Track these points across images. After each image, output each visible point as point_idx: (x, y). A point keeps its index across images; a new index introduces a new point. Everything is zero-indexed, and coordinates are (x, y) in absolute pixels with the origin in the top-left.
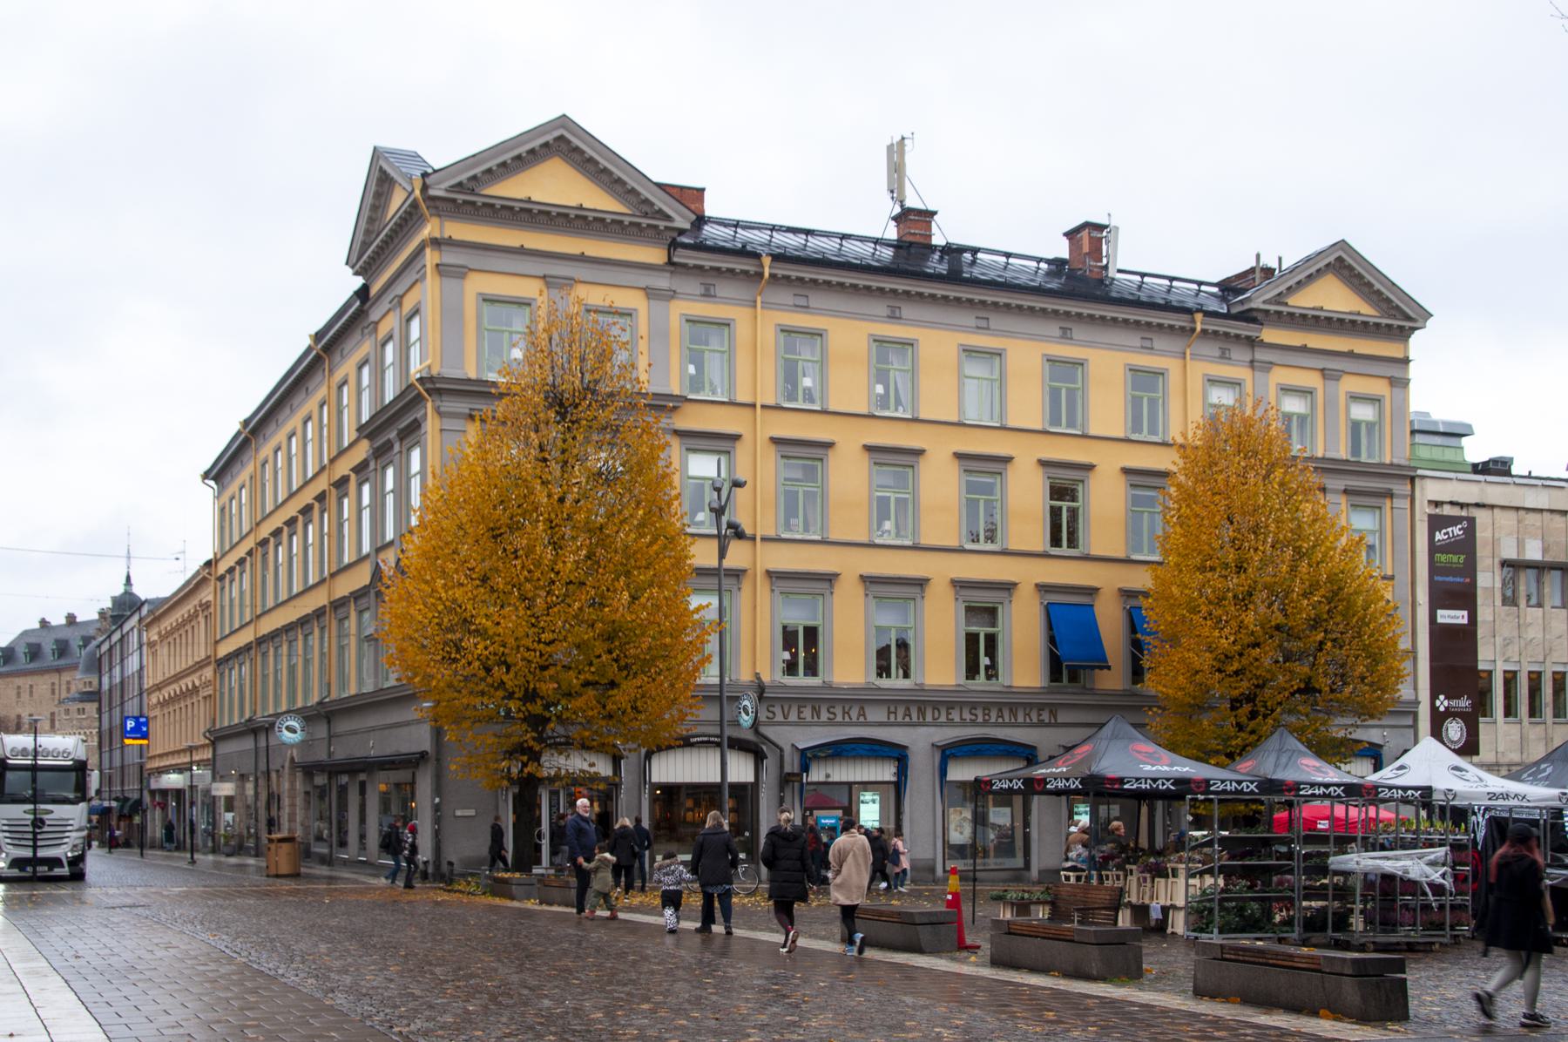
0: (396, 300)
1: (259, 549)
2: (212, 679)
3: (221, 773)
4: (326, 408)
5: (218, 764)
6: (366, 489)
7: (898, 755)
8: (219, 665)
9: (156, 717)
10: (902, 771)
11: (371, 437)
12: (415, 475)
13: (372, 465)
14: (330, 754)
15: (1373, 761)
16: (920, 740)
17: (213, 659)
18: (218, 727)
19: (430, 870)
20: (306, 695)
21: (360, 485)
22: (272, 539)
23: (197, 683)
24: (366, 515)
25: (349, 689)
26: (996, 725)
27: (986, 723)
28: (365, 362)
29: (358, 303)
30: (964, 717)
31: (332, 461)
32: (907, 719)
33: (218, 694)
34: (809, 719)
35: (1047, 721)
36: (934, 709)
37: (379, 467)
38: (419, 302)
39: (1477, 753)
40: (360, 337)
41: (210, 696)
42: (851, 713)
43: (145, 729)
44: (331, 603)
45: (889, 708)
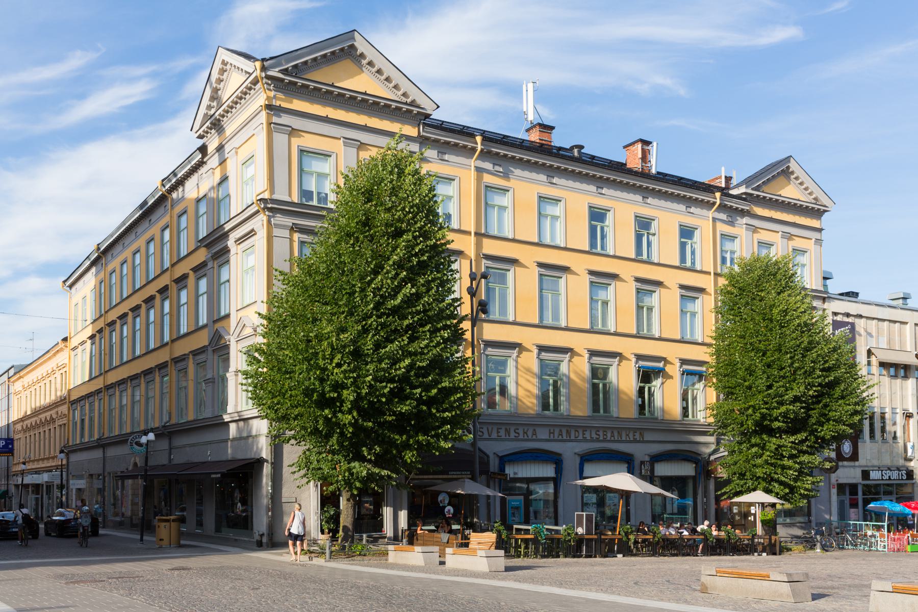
0: (234, 150)
1: (107, 327)
2: (67, 413)
3: (73, 474)
4: (103, 284)
5: (70, 468)
6: (167, 304)
7: (556, 460)
8: (72, 404)
9: (20, 438)
10: (559, 470)
11: (208, 246)
12: (166, 314)
13: (210, 265)
14: (170, 460)
15: (554, 466)
16: (569, 450)
17: (67, 401)
18: (71, 444)
19: (265, 540)
20: (91, 435)
21: (148, 310)
22: (98, 335)
23: (54, 416)
24: (167, 319)
25: (186, 414)
26: (610, 441)
27: (605, 440)
28: (138, 251)
29: (200, 156)
30: (592, 436)
31: (106, 312)
32: (560, 437)
33: (71, 423)
34: (503, 437)
35: (638, 439)
36: (576, 431)
37: (215, 266)
38: (154, 234)
39: (858, 460)
40: (148, 225)
41: (65, 424)
42: (528, 433)
43: (10, 446)
44: (105, 387)
45: (550, 430)
